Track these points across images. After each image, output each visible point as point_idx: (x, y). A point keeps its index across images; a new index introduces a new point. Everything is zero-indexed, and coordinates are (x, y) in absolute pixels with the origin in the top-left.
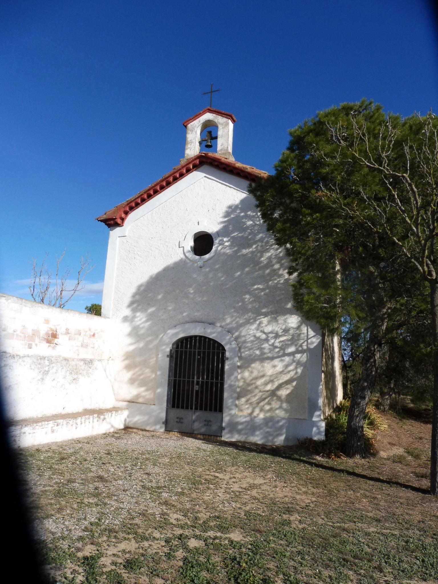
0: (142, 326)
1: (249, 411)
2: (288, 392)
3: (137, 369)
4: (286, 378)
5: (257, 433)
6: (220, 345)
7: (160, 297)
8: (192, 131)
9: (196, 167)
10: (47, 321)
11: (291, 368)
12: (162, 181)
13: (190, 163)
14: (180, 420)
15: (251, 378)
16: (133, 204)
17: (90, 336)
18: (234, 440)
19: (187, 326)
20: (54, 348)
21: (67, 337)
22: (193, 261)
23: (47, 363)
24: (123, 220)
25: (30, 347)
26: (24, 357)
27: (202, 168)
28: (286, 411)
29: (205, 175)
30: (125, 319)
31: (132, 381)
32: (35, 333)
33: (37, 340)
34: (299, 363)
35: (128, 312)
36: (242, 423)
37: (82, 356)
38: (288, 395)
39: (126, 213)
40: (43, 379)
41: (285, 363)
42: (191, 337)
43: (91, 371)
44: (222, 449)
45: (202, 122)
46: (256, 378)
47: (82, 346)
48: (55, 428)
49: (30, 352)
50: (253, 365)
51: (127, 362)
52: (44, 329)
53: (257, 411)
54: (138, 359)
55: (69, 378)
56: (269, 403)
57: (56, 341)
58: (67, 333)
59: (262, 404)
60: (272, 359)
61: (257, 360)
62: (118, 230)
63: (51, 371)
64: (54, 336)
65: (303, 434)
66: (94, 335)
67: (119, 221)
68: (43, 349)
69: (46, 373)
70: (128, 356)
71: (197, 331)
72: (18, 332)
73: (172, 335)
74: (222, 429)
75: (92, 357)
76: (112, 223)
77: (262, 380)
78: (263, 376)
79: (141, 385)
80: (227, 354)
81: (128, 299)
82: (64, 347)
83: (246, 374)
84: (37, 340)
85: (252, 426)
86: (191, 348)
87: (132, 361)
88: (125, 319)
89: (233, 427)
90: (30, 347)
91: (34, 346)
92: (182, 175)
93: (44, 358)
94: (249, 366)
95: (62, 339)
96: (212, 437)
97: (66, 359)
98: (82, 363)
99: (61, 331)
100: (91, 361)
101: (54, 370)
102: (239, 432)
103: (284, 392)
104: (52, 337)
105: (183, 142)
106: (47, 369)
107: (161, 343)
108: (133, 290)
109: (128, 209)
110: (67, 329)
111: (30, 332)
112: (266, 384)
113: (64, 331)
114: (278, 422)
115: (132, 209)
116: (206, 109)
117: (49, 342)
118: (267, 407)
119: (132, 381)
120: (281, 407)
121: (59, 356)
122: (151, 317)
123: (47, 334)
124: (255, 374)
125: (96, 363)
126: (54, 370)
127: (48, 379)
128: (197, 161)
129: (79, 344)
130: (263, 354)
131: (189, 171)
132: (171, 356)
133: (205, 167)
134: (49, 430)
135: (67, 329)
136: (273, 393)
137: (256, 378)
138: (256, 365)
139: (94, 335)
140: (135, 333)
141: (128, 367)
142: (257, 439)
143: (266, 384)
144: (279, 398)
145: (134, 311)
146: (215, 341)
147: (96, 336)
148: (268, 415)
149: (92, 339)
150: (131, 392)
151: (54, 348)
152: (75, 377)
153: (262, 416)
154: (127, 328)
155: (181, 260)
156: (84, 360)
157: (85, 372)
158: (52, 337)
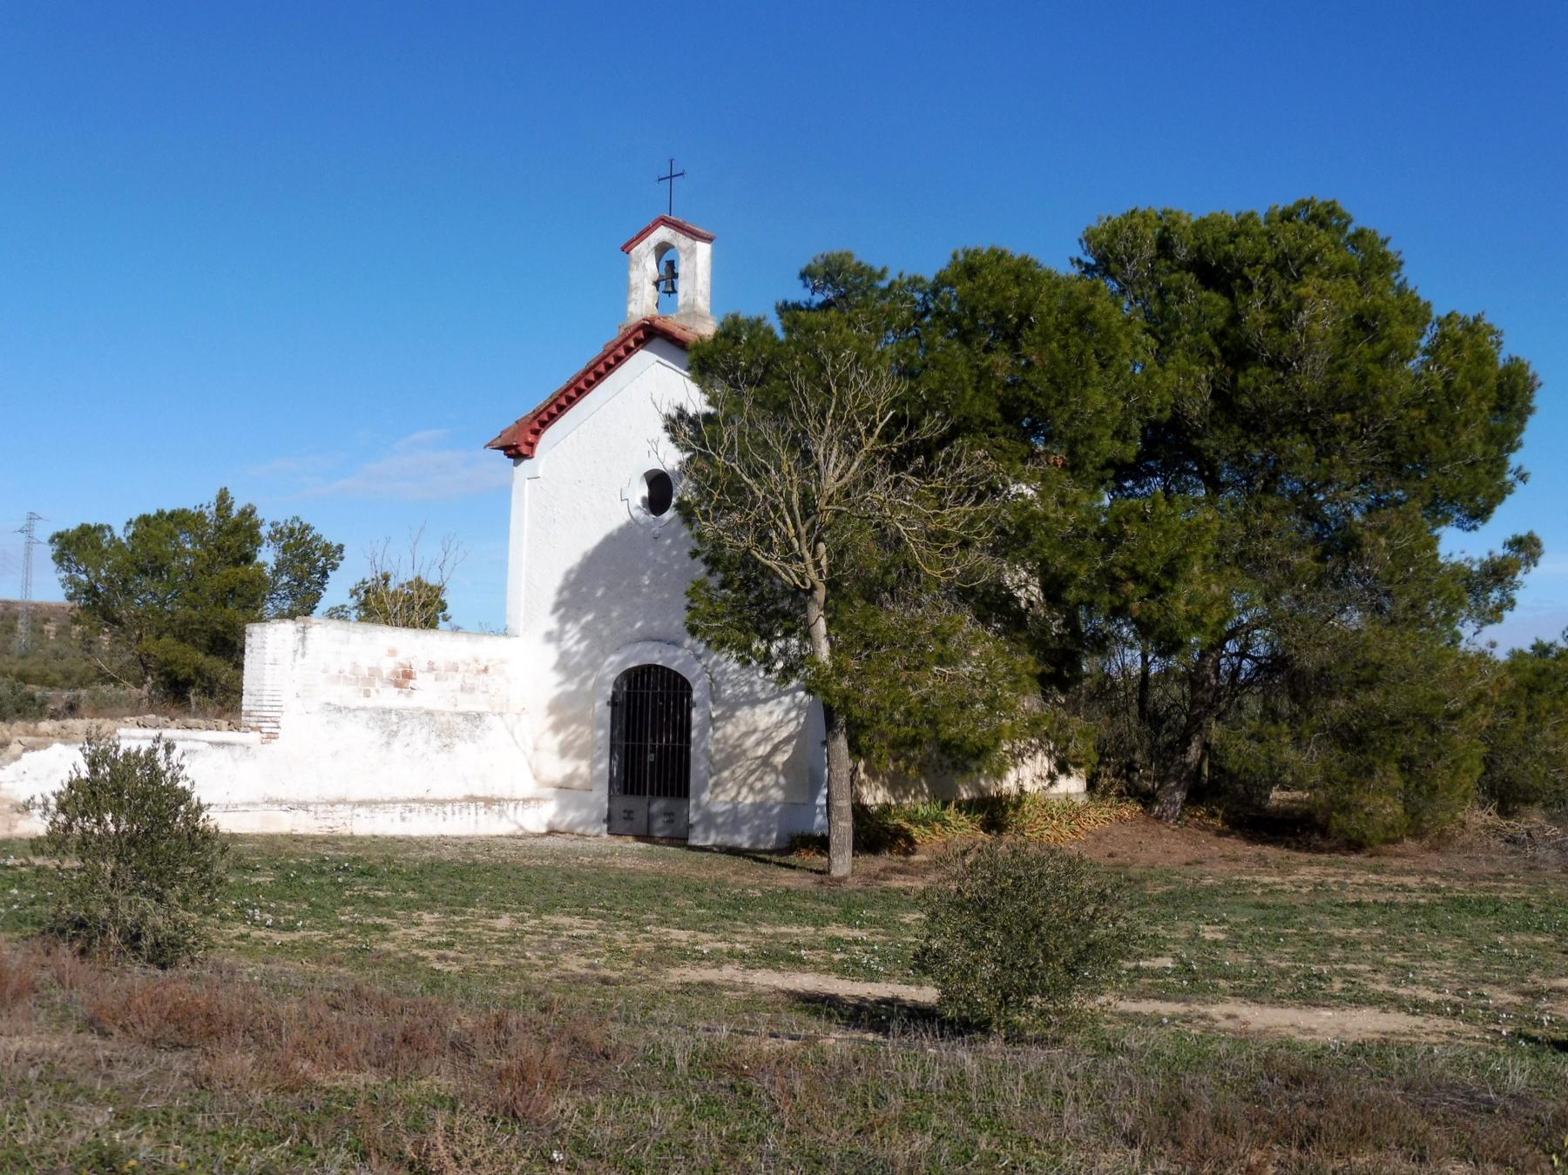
0: (575, 649)
1: (733, 794)
2: (786, 757)
3: (573, 727)
4: (784, 733)
5: (745, 828)
6: (684, 681)
7: (599, 593)
8: (637, 264)
9: (640, 343)
10: (393, 653)
11: (793, 714)
12: (587, 372)
13: (627, 339)
14: (629, 815)
15: (737, 735)
16: (545, 417)
17: (478, 672)
18: (709, 843)
19: (639, 647)
20: (408, 695)
21: (431, 676)
22: (648, 526)
23: (394, 718)
24: (532, 445)
25: (367, 694)
26: (358, 709)
27: (650, 345)
28: (782, 788)
29: (657, 357)
30: (549, 637)
31: (564, 751)
32: (374, 673)
33: (378, 684)
34: (799, 707)
35: (552, 624)
36: (723, 813)
37: (462, 708)
38: (784, 764)
39: (537, 433)
40: (388, 743)
41: (784, 707)
42: (650, 667)
43: (478, 732)
44: (691, 854)
45: (653, 245)
46: (747, 734)
47: (462, 689)
48: (407, 814)
49: (369, 703)
50: (738, 713)
51: (552, 719)
52: (388, 666)
53: (744, 791)
54: (570, 712)
55: (435, 743)
56: (760, 779)
57: (411, 683)
58: (431, 667)
59: (752, 779)
60: (766, 701)
61: (744, 704)
62: (526, 463)
63: (402, 732)
64: (408, 675)
65: (800, 828)
66: (486, 670)
67: (524, 449)
68: (390, 697)
69: (394, 734)
70: (555, 707)
71: (655, 656)
72: (346, 673)
73: (613, 665)
74: (690, 827)
75: (481, 709)
76: (516, 450)
77: (753, 739)
78: (755, 731)
79: (580, 755)
80: (695, 696)
81: (549, 596)
82: (426, 693)
83: (729, 729)
84: (378, 684)
85: (735, 819)
86: (669, 687)
87: (563, 711)
88: (549, 637)
89: (709, 820)
90: (367, 694)
91: (373, 693)
92: (619, 360)
93: (390, 711)
94: (732, 716)
95: (421, 680)
96: (680, 839)
97: (430, 713)
98: (460, 719)
99: (419, 666)
100: (479, 715)
101: (408, 729)
102: (718, 828)
103: (780, 759)
104: (404, 677)
105: (624, 289)
106: (395, 728)
107: (600, 682)
108: (557, 581)
109: (537, 426)
110: (431, 663)
111: (366, 672)
112: (758, 744)
113: (425, 666)
114: (772, 807)
115: (544, 425)
116: (654, 218)
117: (398, 685)
118: (758, 785)
119: (564, 751)
120: (777, 784)
121: (419, 709)
122: (586, 631)
123: (395, 673)
124: (743, 729)
125: (494, 721)
126: (408, 729)
127: (397, 745)
128: (641, 335)
129: (457, 686)
130: (752, 693)
131: (629, 351)
132: (613, 703)
133: (657, 342)
134: (397, 816)
135: (431, 663)
136: (766, 761)
137: (747, 734)
138: (743, 713)
139: (486, 670)
140: (565, 665)
141: (557, 728)
142: (743, 841)
143: (758, 744)
144: (774, 769)
145: (563, 620)
146: (677, 675)
147: (491, 670)
148: (759, 799)
149: (483, 677)
150: (559, 769)
151: (408, 695)
152: (448, 741)
153: (749, 800)
154: (551, 654)
155: (628, 523)
156: (466, 716)
157: (465, 735)
158: (404, 677)
